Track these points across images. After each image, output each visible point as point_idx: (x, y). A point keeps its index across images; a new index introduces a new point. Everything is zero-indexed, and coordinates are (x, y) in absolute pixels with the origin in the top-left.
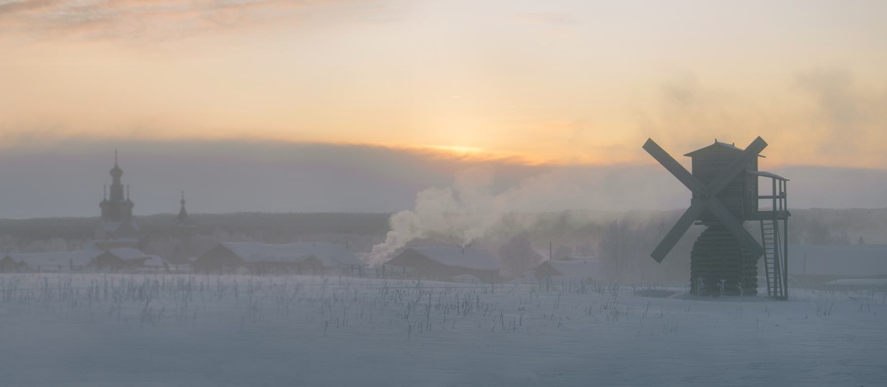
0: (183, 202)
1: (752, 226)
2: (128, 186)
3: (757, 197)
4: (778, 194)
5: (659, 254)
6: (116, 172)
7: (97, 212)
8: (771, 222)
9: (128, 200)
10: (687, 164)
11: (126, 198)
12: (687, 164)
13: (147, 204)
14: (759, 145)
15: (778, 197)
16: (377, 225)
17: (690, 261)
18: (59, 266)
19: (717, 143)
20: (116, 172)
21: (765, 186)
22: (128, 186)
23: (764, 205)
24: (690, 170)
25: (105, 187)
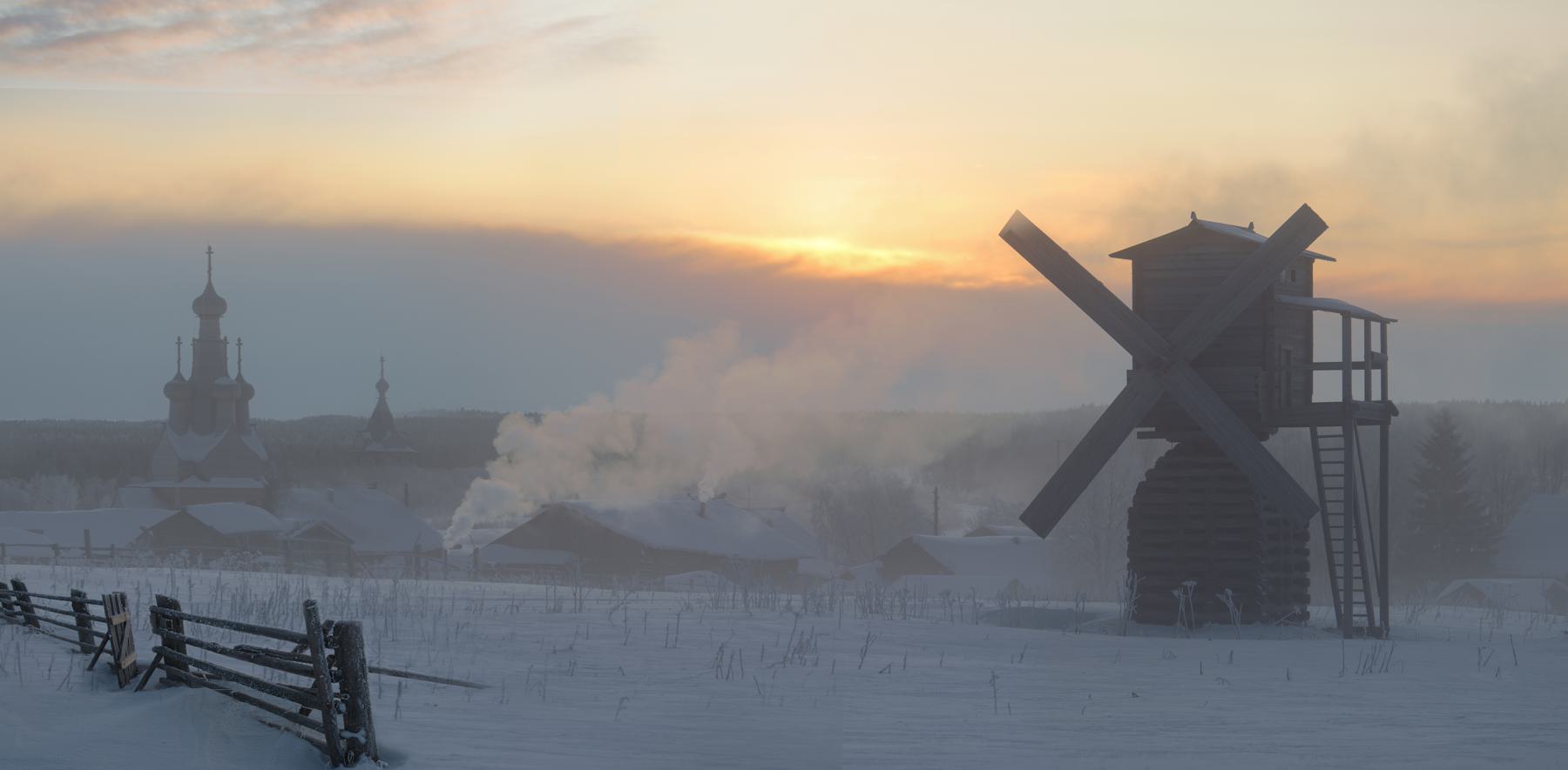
0: (382, 386)
1: (1288, 445)
2: (239, 344)
3: (1308, 366)
4: (1358, 355)
5: (1043, 514)
6: (210, 306)
7: (160, 409)
8: (1338, 430)
9: (240, 377)
10: (1119, 279)
11: (233, 373)
12: (1119, 279)
13: (290, 387)
14: (1306, 224)
15: (1358, 366)
16: (463, 445)
17: (1125, 532)
18: (55, 547)
19: (1196, 225)
20: (210, 306)
21: (1326, 339)
22: (239, 344)
23: (1326, 388)
24: (1127, 299)
25: (179, 343)
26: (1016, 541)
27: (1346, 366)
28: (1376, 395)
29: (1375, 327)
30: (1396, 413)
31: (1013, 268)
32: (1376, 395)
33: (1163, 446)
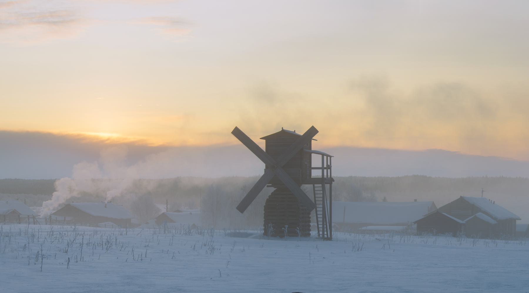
1: (307, 188)
3: (311, 168)
4: (325, 166)
5: (242, 207)
8: (320, 185)
10: (262, 145)
12: (262, 145)
14: (313, 131)
15: (325, 168)
17: (263, 212)
21: (316, 161)
23: (316, 174)
26: (191, 214)
27: (323, 168)
28: (329, 177)
29: (329, 158)
30: (334, 181)
31: (235, 141)
32: (329, 177)
33: (273, 189)
